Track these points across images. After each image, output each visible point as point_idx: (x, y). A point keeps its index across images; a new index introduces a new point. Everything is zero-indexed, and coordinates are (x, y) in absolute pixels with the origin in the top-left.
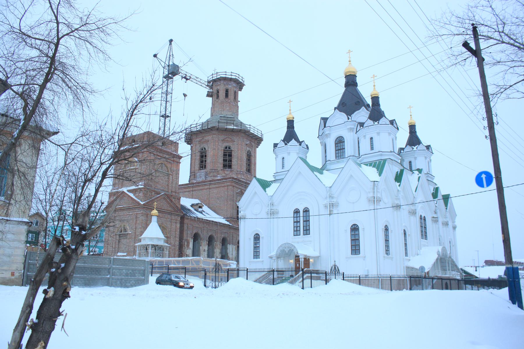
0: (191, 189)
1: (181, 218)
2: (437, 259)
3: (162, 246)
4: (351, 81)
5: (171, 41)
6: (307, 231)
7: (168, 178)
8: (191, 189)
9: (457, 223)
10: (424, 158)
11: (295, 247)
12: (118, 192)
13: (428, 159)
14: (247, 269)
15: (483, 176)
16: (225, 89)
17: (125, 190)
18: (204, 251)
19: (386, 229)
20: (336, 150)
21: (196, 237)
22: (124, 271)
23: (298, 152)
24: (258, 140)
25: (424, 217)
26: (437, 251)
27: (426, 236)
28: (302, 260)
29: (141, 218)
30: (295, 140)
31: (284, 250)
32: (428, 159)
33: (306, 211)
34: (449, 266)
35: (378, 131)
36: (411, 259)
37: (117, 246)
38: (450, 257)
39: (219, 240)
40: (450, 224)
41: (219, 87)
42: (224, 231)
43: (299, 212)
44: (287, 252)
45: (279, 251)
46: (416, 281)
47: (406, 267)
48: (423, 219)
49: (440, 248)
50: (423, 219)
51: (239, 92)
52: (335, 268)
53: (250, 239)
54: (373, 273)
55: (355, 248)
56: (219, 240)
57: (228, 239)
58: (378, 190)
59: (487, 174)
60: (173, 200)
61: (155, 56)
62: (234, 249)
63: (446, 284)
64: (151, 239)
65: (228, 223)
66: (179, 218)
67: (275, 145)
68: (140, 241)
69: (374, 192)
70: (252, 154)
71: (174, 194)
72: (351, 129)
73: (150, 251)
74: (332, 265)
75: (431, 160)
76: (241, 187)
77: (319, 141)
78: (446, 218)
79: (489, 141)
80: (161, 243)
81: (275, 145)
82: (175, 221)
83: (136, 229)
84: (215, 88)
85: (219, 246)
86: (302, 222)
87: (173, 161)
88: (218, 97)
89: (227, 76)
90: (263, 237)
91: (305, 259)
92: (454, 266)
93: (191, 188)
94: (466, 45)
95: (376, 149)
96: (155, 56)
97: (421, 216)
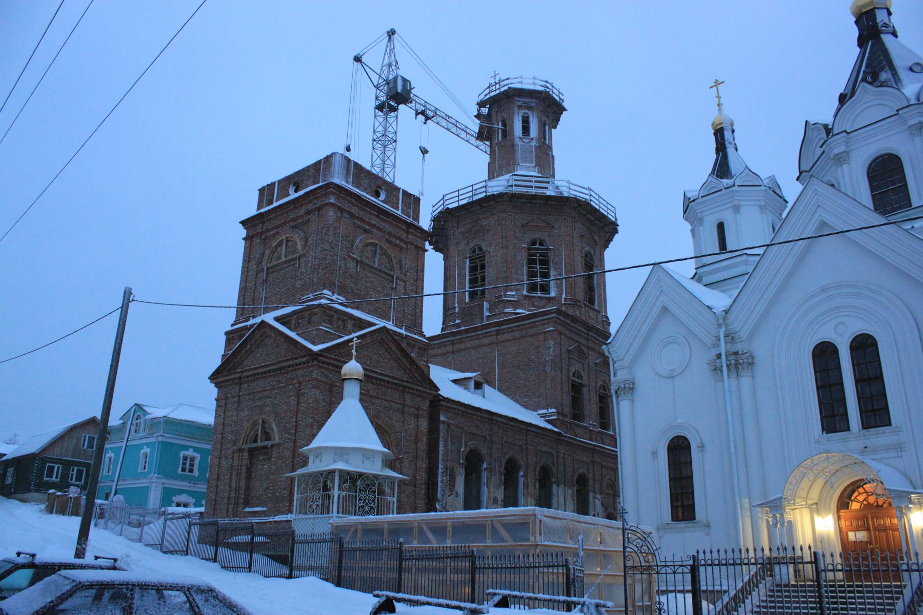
3: (376, 477)
5: (391, 33)
12: (246, 328)
16: (517, 116)
17: (269, 318)
21: (473, 464)
23: (763, 203)
24: (599, 227)
29: (313, 395)
33: (864, 347)
37: (243, 484)
42: (545, 449)
53: (655, 454)
61: (358, 59)
62: (569, 499)
64: (341, 452)
65: (549, 427)
66: (427, 404)
68: (305, 463)
73: (336, 492)
76: (577, 338)
80: (375, 468)
81: (688, 204)
87: (406, 243)
93: (446, 347)
96: (358, 59)
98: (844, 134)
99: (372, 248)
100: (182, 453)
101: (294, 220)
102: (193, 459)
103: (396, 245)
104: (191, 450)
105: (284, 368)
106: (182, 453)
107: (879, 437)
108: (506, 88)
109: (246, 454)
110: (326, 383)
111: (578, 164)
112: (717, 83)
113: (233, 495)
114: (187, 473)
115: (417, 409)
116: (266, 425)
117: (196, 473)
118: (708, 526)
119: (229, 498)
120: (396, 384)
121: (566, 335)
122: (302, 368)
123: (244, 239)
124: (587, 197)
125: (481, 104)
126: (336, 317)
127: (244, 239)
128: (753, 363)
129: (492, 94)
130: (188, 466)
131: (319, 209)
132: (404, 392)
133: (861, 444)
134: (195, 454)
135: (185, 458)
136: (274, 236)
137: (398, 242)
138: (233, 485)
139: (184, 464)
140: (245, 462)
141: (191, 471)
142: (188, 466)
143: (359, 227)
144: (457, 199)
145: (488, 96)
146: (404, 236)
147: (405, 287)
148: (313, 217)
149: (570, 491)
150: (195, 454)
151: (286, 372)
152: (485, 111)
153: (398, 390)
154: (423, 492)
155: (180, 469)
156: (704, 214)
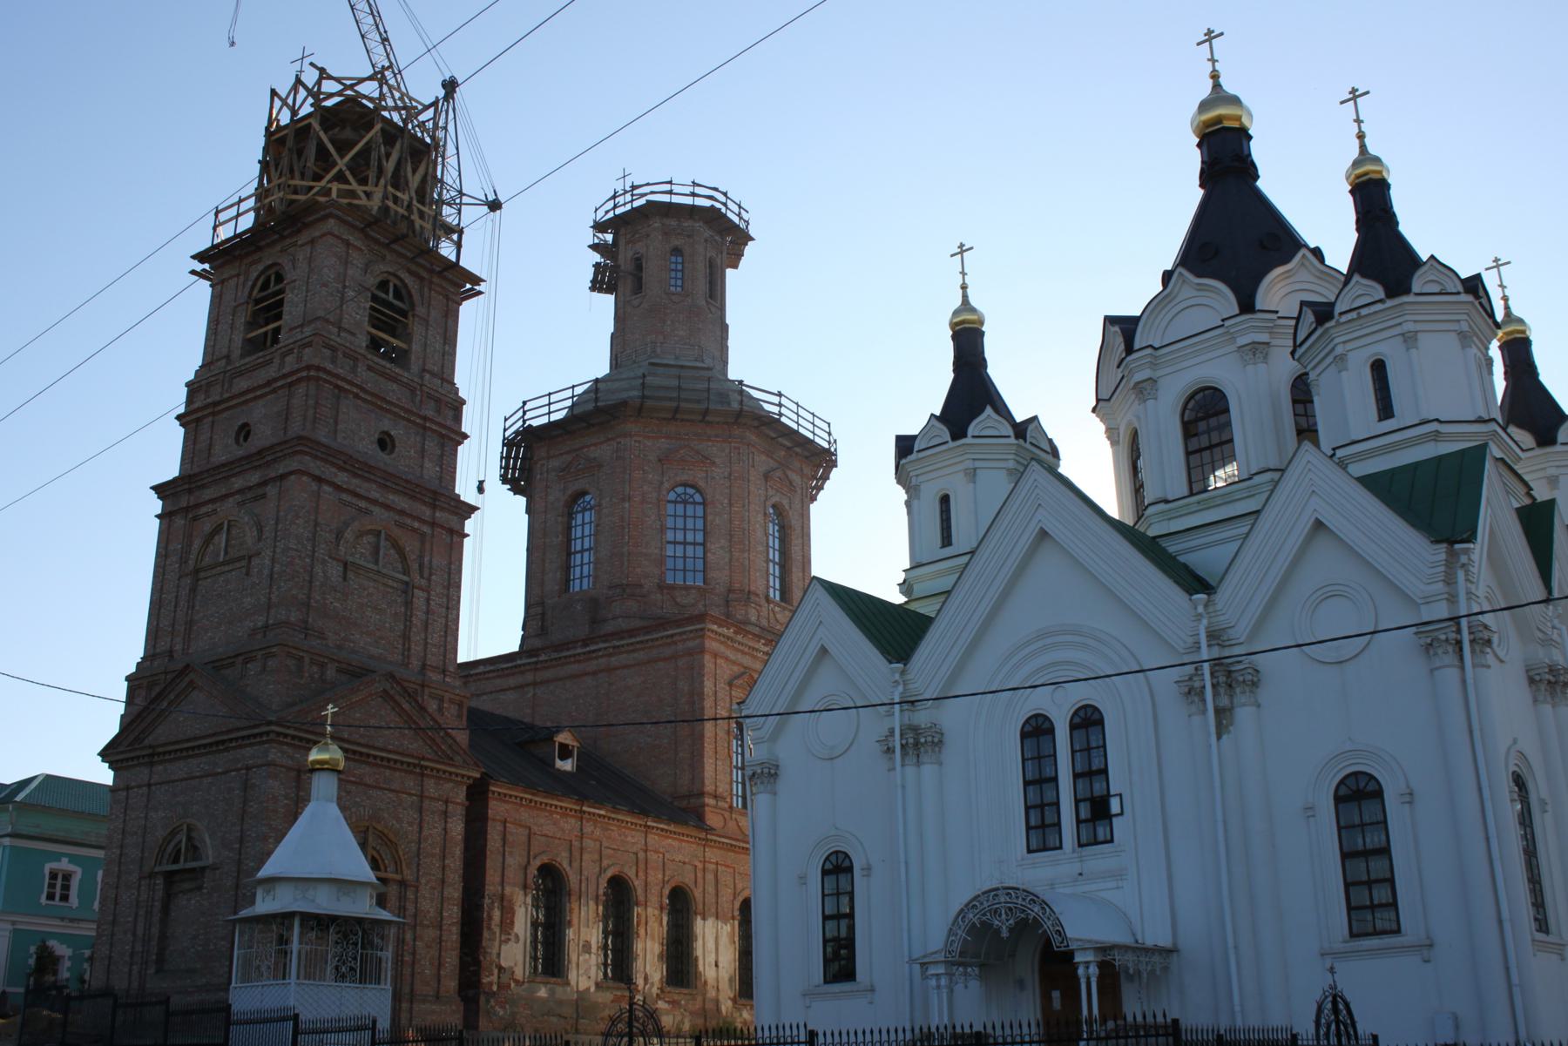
0: (529, 677)
1: (469, 796)
7: (408, 604)
8: (529, 677)
10: (1452, 340)
18: (587, 947)
20: (1188, 454)
28: (1087, 970)
30: (997, 411)
31: (986, 926)
33: (1088, 721)
35: (969, 464)
37: (155, 931)
39: (654, 900)
41: (640, 247)
43: (1051, 731)
51: (729, 272)
53: (803, 880)
56: (654, 900)
57: (698, 893)
60: (432, 706)
67: (904, 445)
70: (795, 522)
71: (435, 677)
73: (295, 945)
74: (1318, 995)
77: (1102, 427)
80: (362, 906)
81: (904, 445)
82: (440, 806)
83: (241, 841)
84: (625, 256)
85: (653, 925)
87: (433, 524)
88: (638, 287)
89: (676, 199)
95: (1405, 411)
98: (1149, 351)
99: (371, 538)
100: (48, 867)
101: (240, 491)
103: (414, 530)
104: (65, 860)
105: (223, 742)
107: (1099, 859)
108: (642, 201)
109: (160, 881)
110: (289, 769)
111: (771, 343)
113: (139, 948)
115: (446, 802)
116: (194, 834)
117: (74, 900)
118: (872, 990)
119: (132, 955)
120: (409, 764)
121: (727, 659)
122: (251, 745)
123: (160, 490)
124: (776, 409)
125: (599, 227)
126: (307, 660)
127: (160, 490)
128: (941, 741)
129: (619, 211)
130: (59, 882)
131: (282, 477)
132: (422, 775)
133: (1077, 868)
134: (71, 867)
135: (53, 876)
136: (207, 514)
137: (416, 525)
138: (140, 932)
139: (51, 886)
140: (159, 894)
141: (65, 898)
142: (59, 882)
143: (350, 504)
144: (546, 410)
145: (611, 215)
146: (427, 512)
147: (428, 600)
148: (271, 490)
149: (728, 928)
150: (71, 867)
151: (227, 750)
152: (609, 237)
153: (411, 772)
154: (454, 937)
155: (44, 896)
156: (921, 479)
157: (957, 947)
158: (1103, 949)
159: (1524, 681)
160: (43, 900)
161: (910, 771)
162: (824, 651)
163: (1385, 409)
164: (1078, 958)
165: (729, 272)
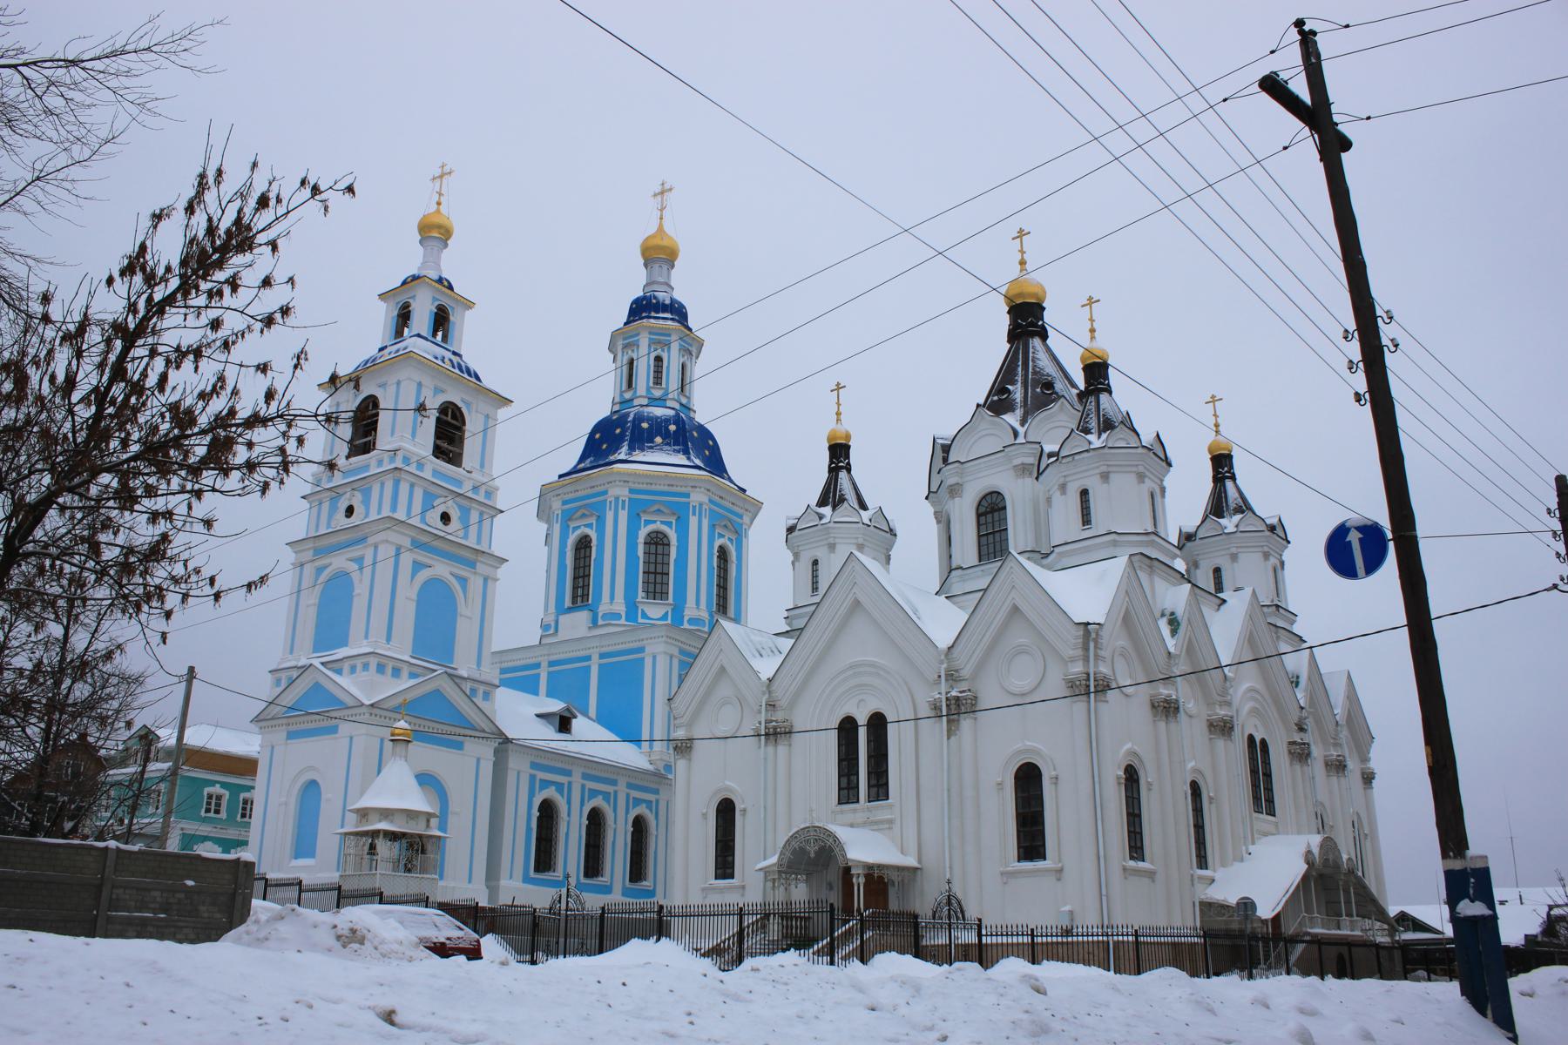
2: (1305, 878)
4: (1026, 319)
6: (880, 788)
9: (1375, 764)
10: (1133, 478)
11: (836, 839)
13: (1273, 561)
14: (661, 907)
15: (1354, 537)
19: (1131, 777)
20: (979, 536)
22: (157, 894)
25: (1263, 742)
26: (1303, 849)
27: (1270, 801)
28: (859, 881)
32: (1273, 561)
33: (878, 723)
34: (1348, 902)
35: (1104, 469)
36: (1217, 876)
38: (1351, 872)
40: (1352, 764)
44: (813, 856)
45: (788, 854)
46: (1232, 945)
47: (1202, 903)
48: (1258, 751)
49: (1315, 840)
50: (1258, 751)
52: (949, 903)
53: (705, 816)
54: (1088, 919)
55: (1031, 842)
58: (1101, 653)
59: (1371, 533)
63: (1340, 958)
69: (1086, 659)
72: (1023, 470)
75: (1282, 563)
77: (932, 510)
78: (1337, 745)
79: (1366, 412)
86: (863, 757)
90: (744, 810)
91: (869, 877)
92: (1370, 906)
94: (1273, 86)
95: (1101, 522)
97: (1251, 738)
100: (207, 790)
102: (219, 798)
106: (207, 790)
107: (881, 810)
112: (1091, 302)
114: (212, 814)
117: (223, 815)
135: (210, 797)
139: (209, 804)
141: (217, 812)
150: (222, 791)
157: (785, 861)
158: (870, 867)
159: (1148, 707)
160: (203, 813)
161: (770, 749)
162: (723, 670)
163: (1086, 519)
164: (853, 871)
165: (1344, 156)
